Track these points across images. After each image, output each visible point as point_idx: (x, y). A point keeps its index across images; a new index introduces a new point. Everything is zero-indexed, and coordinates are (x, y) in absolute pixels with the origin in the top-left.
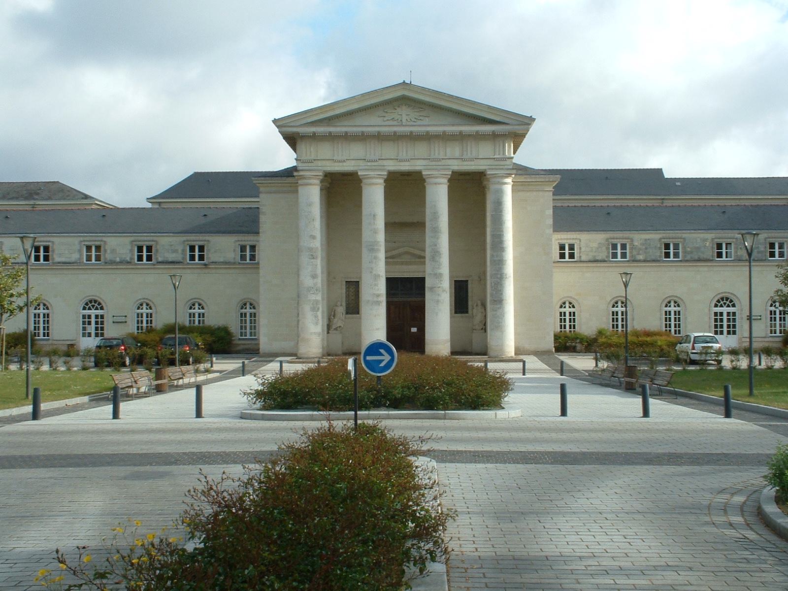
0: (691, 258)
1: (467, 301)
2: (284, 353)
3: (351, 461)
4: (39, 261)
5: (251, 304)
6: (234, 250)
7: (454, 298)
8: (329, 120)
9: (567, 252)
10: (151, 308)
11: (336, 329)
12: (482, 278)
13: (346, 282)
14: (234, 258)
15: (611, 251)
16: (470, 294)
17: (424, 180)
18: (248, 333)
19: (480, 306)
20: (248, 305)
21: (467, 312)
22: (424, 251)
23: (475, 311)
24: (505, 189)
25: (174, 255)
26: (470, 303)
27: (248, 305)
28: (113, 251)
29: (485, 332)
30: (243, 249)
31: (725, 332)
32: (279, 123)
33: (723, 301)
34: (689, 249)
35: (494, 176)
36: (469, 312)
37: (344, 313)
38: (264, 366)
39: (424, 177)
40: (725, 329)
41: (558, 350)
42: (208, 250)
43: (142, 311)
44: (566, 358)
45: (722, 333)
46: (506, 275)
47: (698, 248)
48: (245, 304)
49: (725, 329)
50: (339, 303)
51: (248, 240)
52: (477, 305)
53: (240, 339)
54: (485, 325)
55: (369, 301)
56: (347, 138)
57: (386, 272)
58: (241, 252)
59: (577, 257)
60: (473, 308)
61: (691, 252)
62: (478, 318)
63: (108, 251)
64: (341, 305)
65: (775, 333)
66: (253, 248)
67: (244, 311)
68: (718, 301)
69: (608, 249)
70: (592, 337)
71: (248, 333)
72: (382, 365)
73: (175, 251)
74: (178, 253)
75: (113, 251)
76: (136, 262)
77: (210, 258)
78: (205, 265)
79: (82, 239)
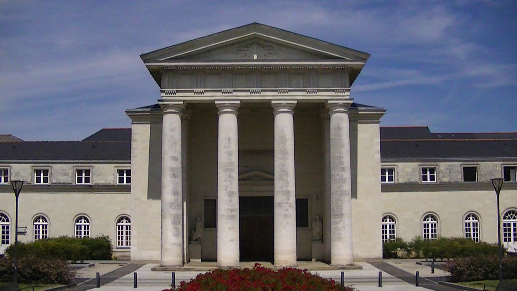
0: (485, 180)
2: (151, 261)
6: (114, 175)
10: (46, 221)
13: (205, 200)
18: (124, 243)
23: (314, 224)
25: (65, 178)
28: (17, 174)
29: (323, 242)
31: (512, 239)
33: (510, 214)
34: (483, 173)
35: (279, 105)
36: (309, 226)
39: (217, 107)
40: (512, 237)
41: (385, 257)
42: (93, 174)
44: (391, 262)
45: (510, 240)
47: (491, 172)
49: (512, 237)
50: (199, 219)
52: (316, 220)
53: (117, 248)
55: (224, 215)
61: (485, 175)
63: (13, 175)
64: (201, 220)
65: (122, 245)
68: (506, 214)
69: (419, 173)
73: (66, 174)
74: (68, 175)
75: (17, 174)
77: (94, 180)
78: (90, 186)
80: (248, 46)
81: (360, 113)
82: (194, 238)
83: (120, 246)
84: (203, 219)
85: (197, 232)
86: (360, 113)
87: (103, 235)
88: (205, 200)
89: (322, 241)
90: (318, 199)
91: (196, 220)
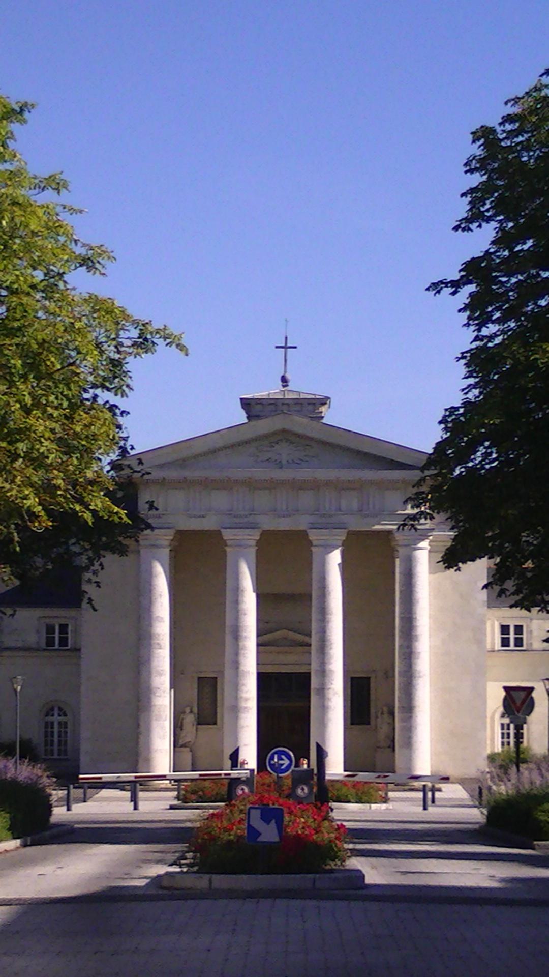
1: (368, 705)
3: (528, 335)
4: (54, 646)
5: (60, 709)
7: (349, 702)
8: (183, 463)
9: (512, 636)
12: (389, 674)
14: (38, 643)
16: (372, 697)
18: (56, 752)
19: (386, 716)
20: (56, 710)
22: (310, 635)
24: (419, 556)
26: (373, 711)
27: (56, 710)
30: (50, 629)
37: (195, 723)
38: (97, 793)
46: (420, 672)
48: (52, 709)
51: (58, 615)
52: (382, 714)
56: (208, 484)
57: (258, 664)
58: (47, 633)
59: (527, 644)
60: (377, 717)
62: (384, 729)
67: (50, 719)
70: (539, 756)
71: (56, 752)
72: (283, 767)
80: (273, 444)
81: (81, 781)
82: (181, 742)
83: (62, 757)
84: (195, 710)
85: (184, 732)
86: (81, 781)
87: (245, 745)
88: (199, 678)
89: (391, 749)
90: (387, 677)
91: (184, 713)
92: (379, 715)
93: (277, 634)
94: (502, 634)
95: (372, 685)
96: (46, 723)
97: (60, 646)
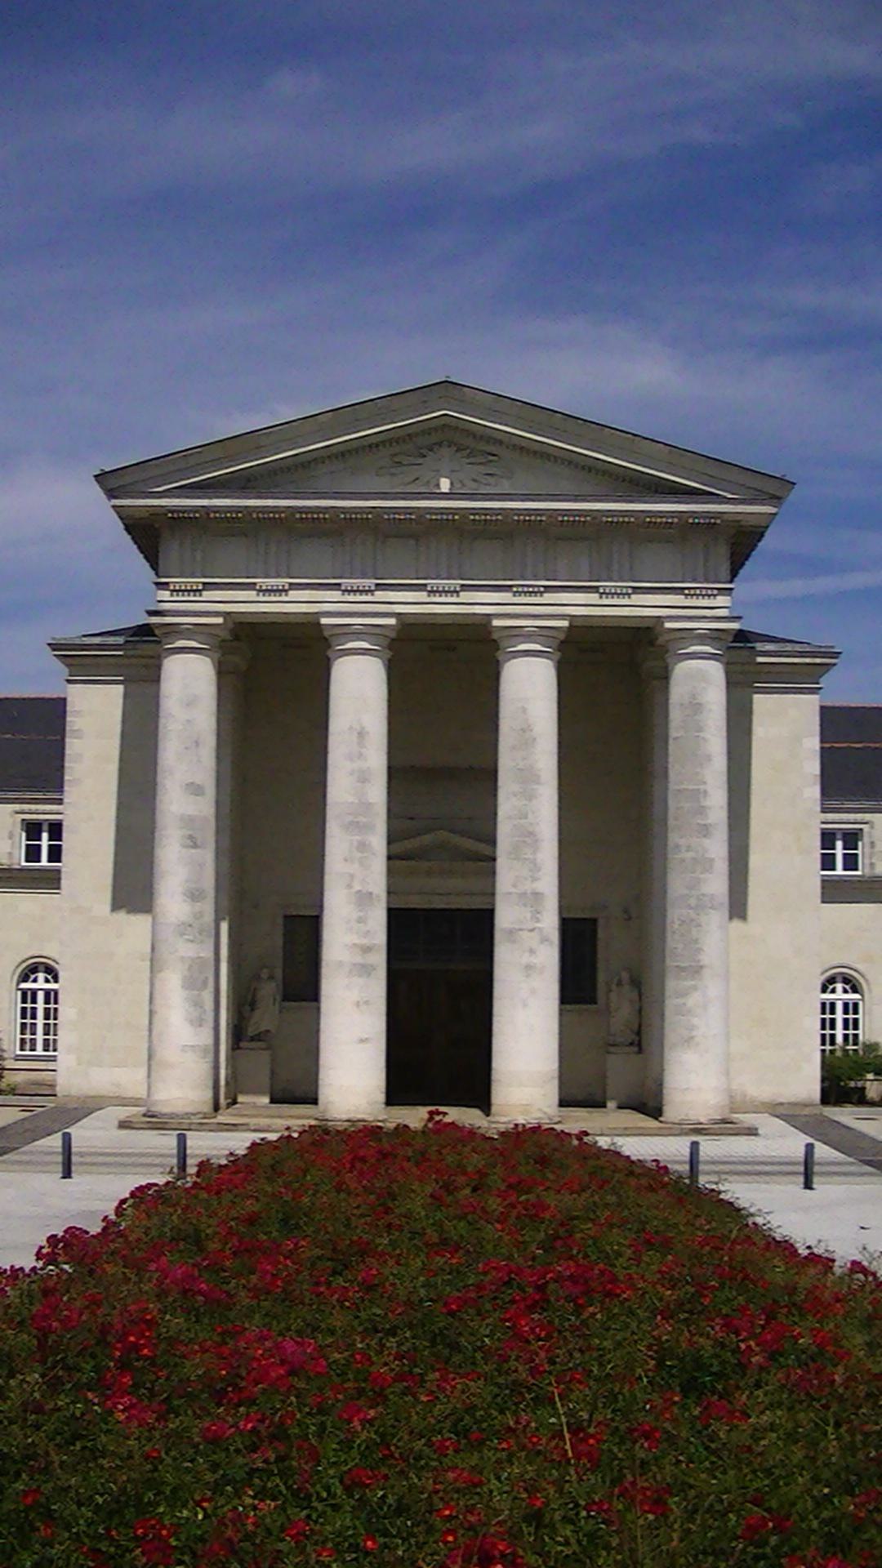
4: (39, 861)
11: (256, 1038)
13: (286, 917)
15: (859, 852)
17: (495, 645)
21: (594, 1001)
23: (613, 996)
26: (601, 977)
32: (114, 483)
37: (279, 998)
39: (326, 633)
43: (832, 996)
50: (265, 974)
54: (639, 1033)
64: (271, 977)
66: (56, 830)
76: (24, 864)
79: (17, 807)
82: (251, 1031)
84: (279, 973)
85: (257, 1013)
92: (614, 987)
93: (427, 839)
94: (60, 846)
95: (601, 934)
96: (24, 993)
97: (49, 861)
